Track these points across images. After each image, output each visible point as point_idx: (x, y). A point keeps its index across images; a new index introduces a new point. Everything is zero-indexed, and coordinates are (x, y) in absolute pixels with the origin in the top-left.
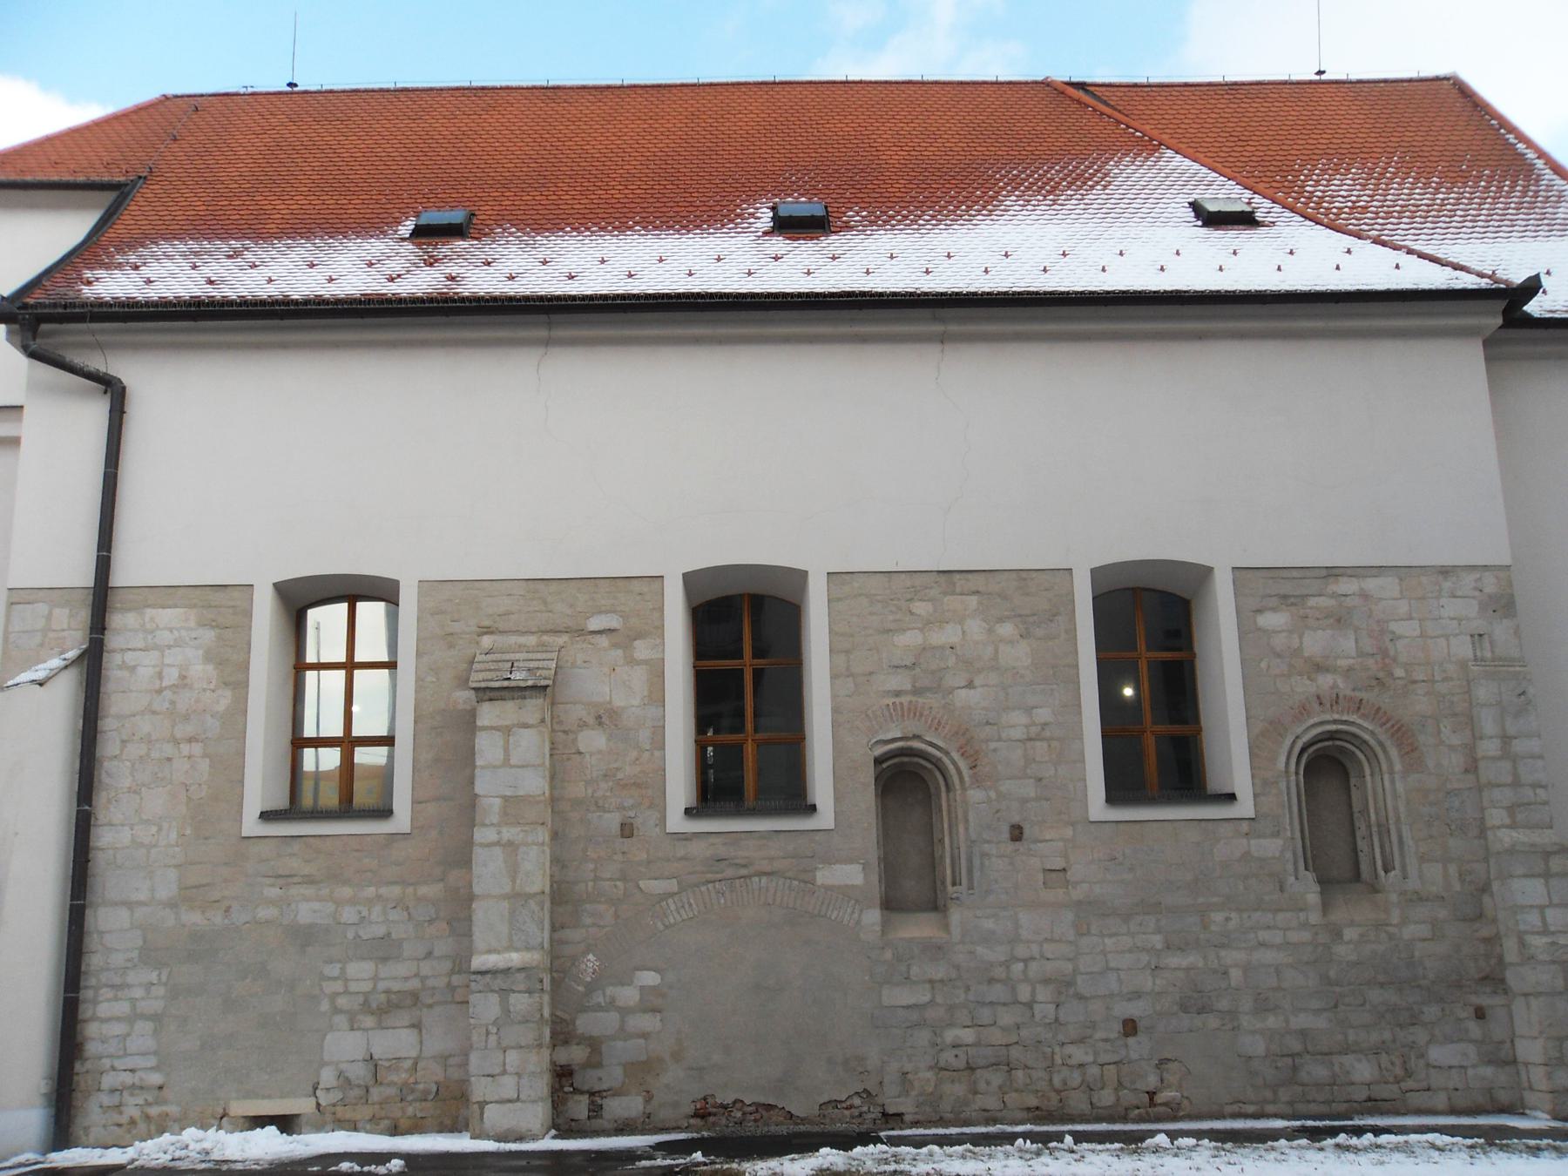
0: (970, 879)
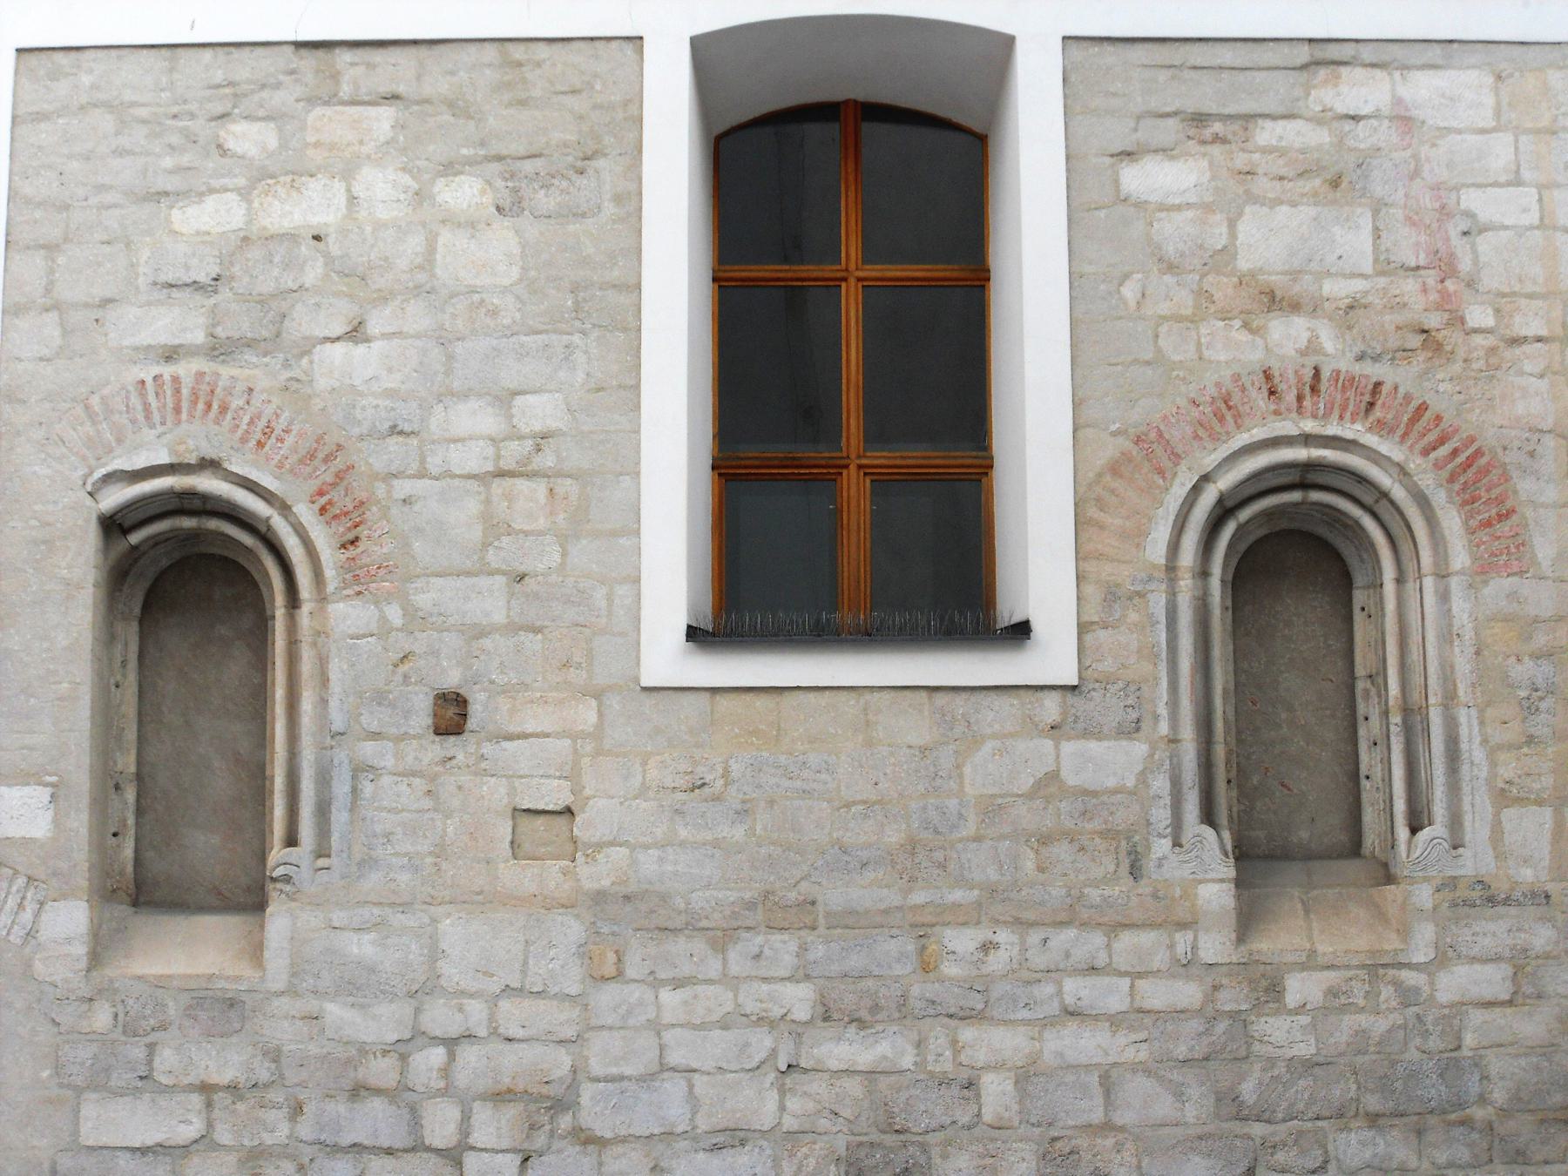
0: (323, 831)
